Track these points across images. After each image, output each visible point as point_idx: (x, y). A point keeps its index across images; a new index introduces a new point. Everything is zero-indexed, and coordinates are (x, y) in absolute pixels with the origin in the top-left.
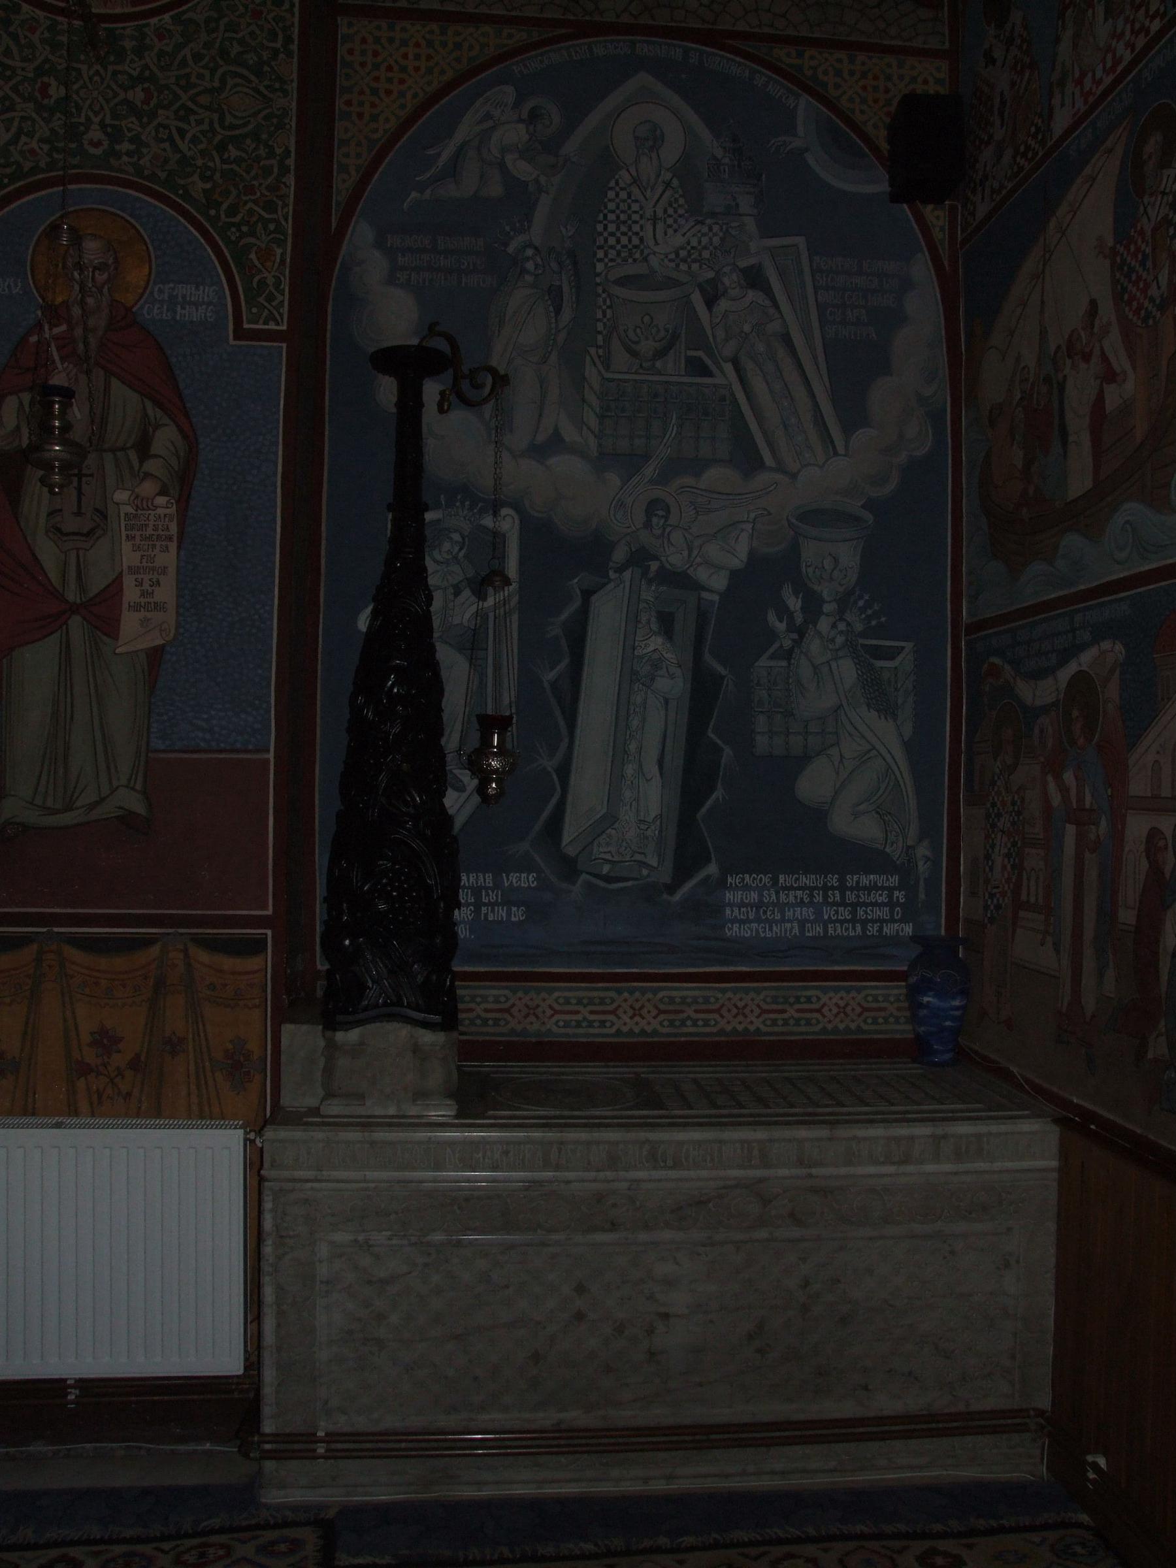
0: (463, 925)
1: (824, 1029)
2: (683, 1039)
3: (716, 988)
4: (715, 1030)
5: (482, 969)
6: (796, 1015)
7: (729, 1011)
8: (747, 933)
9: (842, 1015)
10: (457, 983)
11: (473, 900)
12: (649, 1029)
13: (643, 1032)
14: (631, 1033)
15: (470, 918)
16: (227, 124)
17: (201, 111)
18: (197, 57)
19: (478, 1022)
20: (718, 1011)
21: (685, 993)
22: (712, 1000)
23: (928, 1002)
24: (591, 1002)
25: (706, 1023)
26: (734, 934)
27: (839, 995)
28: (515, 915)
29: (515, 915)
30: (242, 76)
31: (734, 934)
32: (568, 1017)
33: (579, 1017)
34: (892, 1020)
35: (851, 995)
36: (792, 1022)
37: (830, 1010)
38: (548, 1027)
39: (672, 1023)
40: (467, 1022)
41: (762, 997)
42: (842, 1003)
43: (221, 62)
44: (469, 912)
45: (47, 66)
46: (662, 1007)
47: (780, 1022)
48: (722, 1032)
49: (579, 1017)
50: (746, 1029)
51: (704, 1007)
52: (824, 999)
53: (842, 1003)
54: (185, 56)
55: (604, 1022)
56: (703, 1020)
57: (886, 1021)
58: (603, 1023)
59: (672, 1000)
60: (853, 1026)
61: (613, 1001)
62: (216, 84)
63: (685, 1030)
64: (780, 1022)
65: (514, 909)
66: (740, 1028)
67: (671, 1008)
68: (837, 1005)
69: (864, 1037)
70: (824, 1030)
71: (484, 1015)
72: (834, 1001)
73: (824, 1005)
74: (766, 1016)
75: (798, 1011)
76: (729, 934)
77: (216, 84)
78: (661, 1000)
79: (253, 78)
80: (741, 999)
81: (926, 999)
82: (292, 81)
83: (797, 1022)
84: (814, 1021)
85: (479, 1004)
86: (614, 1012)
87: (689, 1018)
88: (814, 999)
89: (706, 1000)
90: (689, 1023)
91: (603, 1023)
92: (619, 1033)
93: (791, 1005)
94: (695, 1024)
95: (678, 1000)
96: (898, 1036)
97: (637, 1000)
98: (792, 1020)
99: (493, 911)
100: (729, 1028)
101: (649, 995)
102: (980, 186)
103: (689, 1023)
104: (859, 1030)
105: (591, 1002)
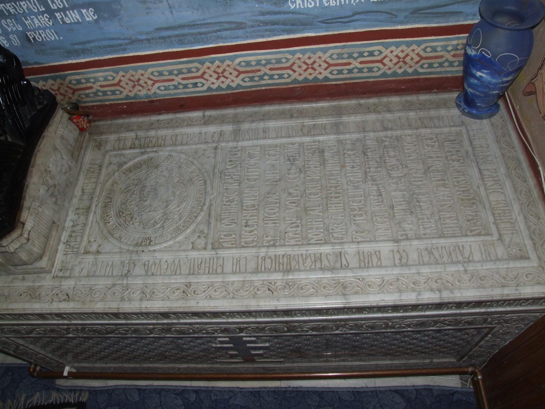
0: (48, 30)
2: (264, 88)
3: (287, 52)
4: (289, 80)
5: (83, 60)
6: (360, 66)
8: (311, 4)
9: (401, 63)
11: (44, 9)
12: (234, 85)
13: (229, 87)
14: (219, 88)
15: (51, 24)
19: (100, 94)
20: (290, 68)
21: (259, 57)
22: (284, 60)
23: (481, 76)
24: (180, 72)
25: (281, 76)
26: (298, 7)
27: (400, 49)
28: (87, 16)
29: (87, 16)
31: (298, 7)
32: (166, 84)
35: (402, 70)
36: (356, 70)
37: (391, 60)
38: (153, 91)
41: (328, 54)
42: (402, 55)
44: (46, 20)
46: (241, 69)
47: (345, 72)
48: (295, 81)
50: (316, 78)
51: (277, 66)
52: (386, 52)
53: (402, 55)
55: (196, 84)
56: (278, 75)
58: (195, 85)
59: (248, 63)
60: (410, 71)
61: (198, 70)
63: (263, 82)
64: (345, 72)
65: (84, 11)
66: (310, 78)
67: (249, 69)
68: (397, 56)
70: (384, 75)
71: (101, 89)
72: (395, 53)
74: (332, 68)
75: (361, 63)
76: (292, 7)
78: (239, 64)
80: (309, 58)
81: (479, 74)
83: (360, 70)
85: (94, 83)
86: (202, 76)
87: (265, 74)
88: (376, 53)
89: (279, 61)
90: (266, 77)
91: (195, 85)
92: (209, 89)
93: (355, 59)
94: (271, 77)
95: (253, 63)
96: (450, 75)
97: (219, 67)
98: (356, 69)
99: (66, 15)
100: (301, 78)
101: (228, 62)
102: (420, 203)
103: (266, 77)
104: (416, 72)
105: (180, 72)
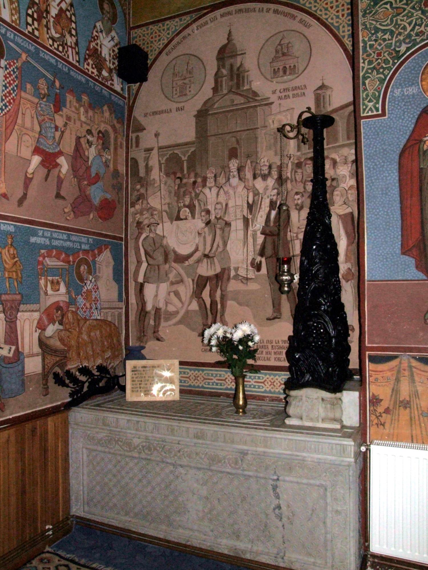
1: (280, 376)
7: (268, 383)
10: (234, 392)
16: (389, 5)
17: (401, 6)
18: (404, 28)
30: (384, 26)
33: (217, 378)
34: (214, 375)
39: (220, 376)
40: (248, 377)
43: (393, 29)
45: (410, 14)
49: (254, 380)
54: (410, 26)
57: (216, 375)
62: (394, 19)
64: (257, 378)
69: (189, 367)
73: (203, 381)
77: (394, 19)
79: (379, 26)
82: (362, 30)
84: (206, 375)
86: (263, 383)
90: (214, 375)
